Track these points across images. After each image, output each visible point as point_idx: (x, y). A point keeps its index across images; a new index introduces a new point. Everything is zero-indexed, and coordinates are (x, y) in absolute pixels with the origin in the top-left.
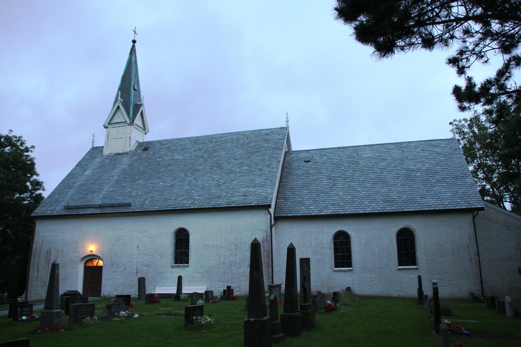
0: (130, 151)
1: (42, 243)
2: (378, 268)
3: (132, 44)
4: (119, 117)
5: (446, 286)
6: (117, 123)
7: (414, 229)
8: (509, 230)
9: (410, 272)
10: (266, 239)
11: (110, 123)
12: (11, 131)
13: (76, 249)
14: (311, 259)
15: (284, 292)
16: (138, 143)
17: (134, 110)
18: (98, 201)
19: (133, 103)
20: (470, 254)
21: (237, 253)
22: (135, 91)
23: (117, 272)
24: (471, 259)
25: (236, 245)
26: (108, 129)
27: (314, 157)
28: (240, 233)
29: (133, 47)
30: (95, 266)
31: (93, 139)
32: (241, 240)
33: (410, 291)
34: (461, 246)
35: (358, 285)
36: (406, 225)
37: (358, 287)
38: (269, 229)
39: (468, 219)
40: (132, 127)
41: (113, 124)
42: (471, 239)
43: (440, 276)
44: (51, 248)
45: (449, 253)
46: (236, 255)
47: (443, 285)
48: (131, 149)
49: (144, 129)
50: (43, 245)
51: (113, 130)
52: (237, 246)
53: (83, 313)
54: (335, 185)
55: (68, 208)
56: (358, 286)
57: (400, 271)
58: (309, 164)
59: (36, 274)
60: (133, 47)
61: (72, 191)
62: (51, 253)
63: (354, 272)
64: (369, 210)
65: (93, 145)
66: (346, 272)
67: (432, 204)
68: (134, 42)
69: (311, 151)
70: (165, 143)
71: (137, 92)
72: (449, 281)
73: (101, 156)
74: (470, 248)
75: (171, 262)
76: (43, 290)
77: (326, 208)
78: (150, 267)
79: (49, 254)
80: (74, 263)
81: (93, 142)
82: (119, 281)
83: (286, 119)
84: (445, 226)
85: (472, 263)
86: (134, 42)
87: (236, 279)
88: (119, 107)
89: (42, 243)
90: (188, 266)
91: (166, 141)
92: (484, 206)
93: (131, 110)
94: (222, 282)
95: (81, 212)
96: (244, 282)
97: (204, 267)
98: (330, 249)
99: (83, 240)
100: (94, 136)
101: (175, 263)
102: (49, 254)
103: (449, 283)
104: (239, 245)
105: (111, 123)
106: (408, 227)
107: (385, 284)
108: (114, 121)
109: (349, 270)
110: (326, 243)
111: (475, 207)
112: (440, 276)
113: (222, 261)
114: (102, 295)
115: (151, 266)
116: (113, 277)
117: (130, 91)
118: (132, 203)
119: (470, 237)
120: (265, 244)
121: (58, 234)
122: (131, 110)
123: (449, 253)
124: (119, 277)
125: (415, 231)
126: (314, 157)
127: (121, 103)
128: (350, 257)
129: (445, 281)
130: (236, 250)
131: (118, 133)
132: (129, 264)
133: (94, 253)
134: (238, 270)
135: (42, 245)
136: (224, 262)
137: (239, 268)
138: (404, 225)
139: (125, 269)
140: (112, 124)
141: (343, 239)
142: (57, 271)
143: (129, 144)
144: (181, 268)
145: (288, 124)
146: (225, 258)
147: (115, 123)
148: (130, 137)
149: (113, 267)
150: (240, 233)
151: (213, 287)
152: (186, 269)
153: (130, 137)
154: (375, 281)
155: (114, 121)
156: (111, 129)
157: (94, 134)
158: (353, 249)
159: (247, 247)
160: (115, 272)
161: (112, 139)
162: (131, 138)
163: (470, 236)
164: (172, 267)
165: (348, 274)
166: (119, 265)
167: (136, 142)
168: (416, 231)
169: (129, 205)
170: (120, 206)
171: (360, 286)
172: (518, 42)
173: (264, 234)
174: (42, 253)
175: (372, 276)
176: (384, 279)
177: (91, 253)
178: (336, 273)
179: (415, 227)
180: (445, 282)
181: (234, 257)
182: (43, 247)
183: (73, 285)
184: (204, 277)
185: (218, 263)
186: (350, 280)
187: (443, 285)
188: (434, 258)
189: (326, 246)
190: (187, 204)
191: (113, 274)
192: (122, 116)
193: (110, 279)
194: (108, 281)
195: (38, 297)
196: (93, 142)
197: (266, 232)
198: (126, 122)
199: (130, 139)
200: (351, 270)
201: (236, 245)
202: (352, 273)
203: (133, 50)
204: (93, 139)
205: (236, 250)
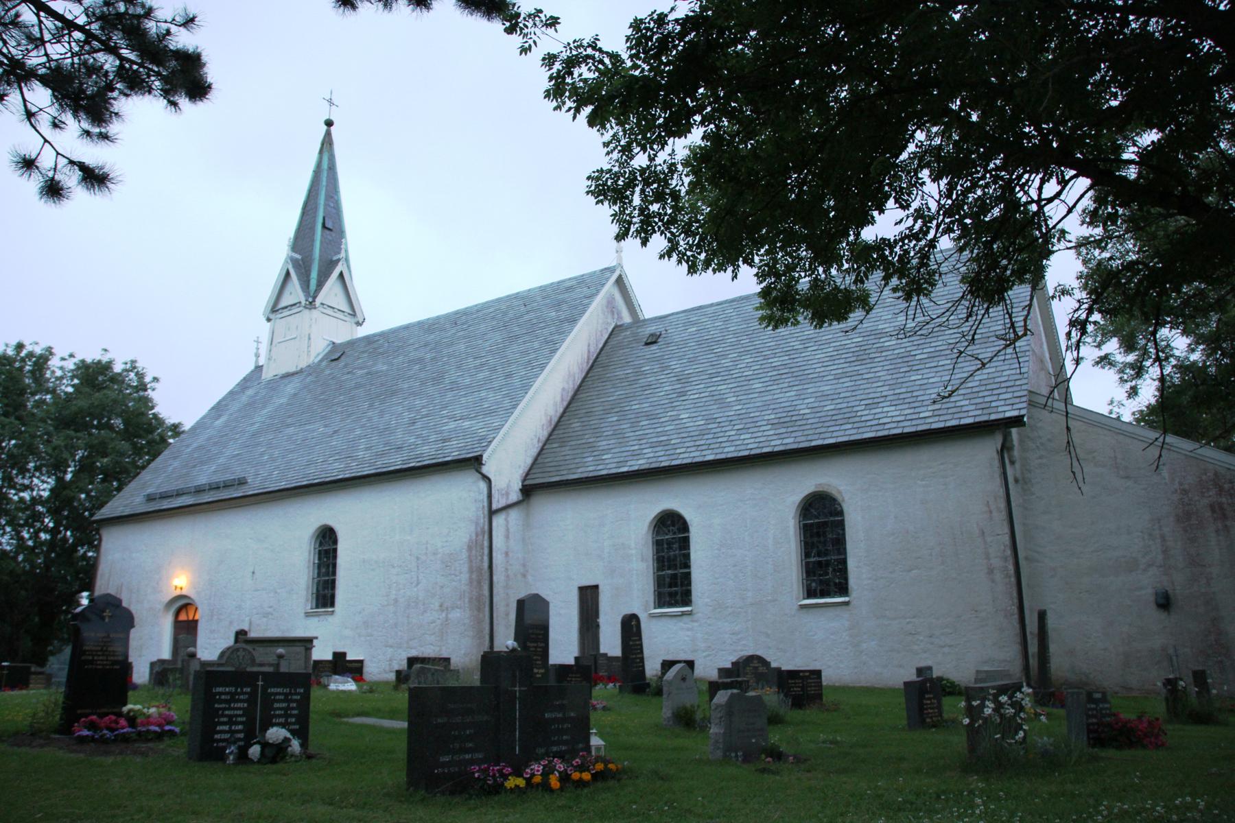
0: (309, 366)
2: (752, 604)
3: (325, 127)
4: (291, 293)
5: (925, 652)
6: (286, 307)
7: (840, 492)
8: (1127, 477)
9: (831, 612)
10: (476, 541)
11: (275, 309)
12: (106, 350)
14: (601, 588)
15: (406, 666)
16: (332, 345)
17: (319, 275)
18: (202, 479)
19: (320, 260)
20: (988, 557)
21: (420, 578)
22: (328, 232)
24: (991, 571)
25: (418, 558)
26: (272, 321)
27: (669, 331)
28: (428, 528)
29: (328, 135)
31: (258, 349)
32: (428, 546)
33: (830, 667)
34: (962, 534)
35: (704, 652)
36: (820, 484)
37: (705, 657)
38: (487, 520)
39: (985, 451)
40: (315, 313)
42: (991, 512)
43: (908, 623)
45: (931, 555)
46: (418, 584)
47: (916, 647)
48: (310, 361)
49: (354, 314)
51: (280, 323)
52: (419, 562)
53: (457, 745)
54: (683, 394)
55: (150, 498)
56: (704, 654)
57: (805, 610)
58: (652, 349)
60: (328, 135)
61: (176, 464)
63: (695, 617)
64: (730, 451)
65: (257, 361)
66: (679, 618)
67: (894, 419)
68: (329, 123)
69: (669, 318)
70: (377, 338)
71: (334, 235)
72: (931, 637)
73: (259, 384)
74: (989, 539)
75: (306, 605)
77: (636, 455)
78: (270, 616)
83: (255, 351)
84: (922, 480)
85: (993, 581)
86: (329, 123)
87: (416, 641)
90: (333, 611)
91: (374, 335)
92: (1023, 412)
93: (314, 275)
94: (391, 647)
95: (166, 505)
96: (432, 647)
97: (360, 613)
98: (642, 561)
100: (258, 342)
101: (317, 607)
103: (932, 644)
104: (423, 558)
106: (825, 489)
107: (769, 648)
108: (283, 303)
109: (683, 614)
110: (633, 545)
111: (1001, 416)
112: (908, 623)
113: (394, 597)
115: (272, 614)
117: (314, 234)
119: (989, 507)
120: (474, 552)
122: (314, 275)
123: (931, 555)
125: (843, 500)
126: (669, 331)
128: (687, 578)
129: (922, 638)
130: (418, 569)
133: (184, 592)
134: (421, 617)
136: (396, 601)
137: (422, 614)
138: (816, 486)
140: (278, 310)
141: (675, 533)
142: (945, 682)
143: (306, 350)
144: (322, 618)
145: (620, 258)
146: (399, 590)
147: (283, 308)
148: (309, 335)
150: (428, 528)
151: (374, 660)
152: (330, 618)
153: (309, 335)
154: (744, 642)
155: (283, 303)
156: (278, 321)
157: (258, 337)
158: (851, 564)
159: (439, 562)
162: (312, 337)
163: (988, 504)
164: (308, 615)
165: (681, 624)
167: (329, 345)
168: (846, 499)
169: (242, 482)
170: (227, 485)
171: (709, 655)
172: (143, 6)
173: (473, 528)
175: (736, 628)
176: (768, 635)
177: (178, 592)
178: (654, 621)
179: (841, 488)
180: (922, 641)
181: (415, 587)
184: (360, 636)
185: (386, 603)
186: (686, 638)
187: (916, 647)
188: (891, 572)
189: (634, 552)
190: (338, 470)
192: (295, 293)
197: (477, 524)
199: (309, 339)
200: (690, 613)
201: (418, 558)
202: (693, 621)
204: (258, 349)
205: (418, 569)
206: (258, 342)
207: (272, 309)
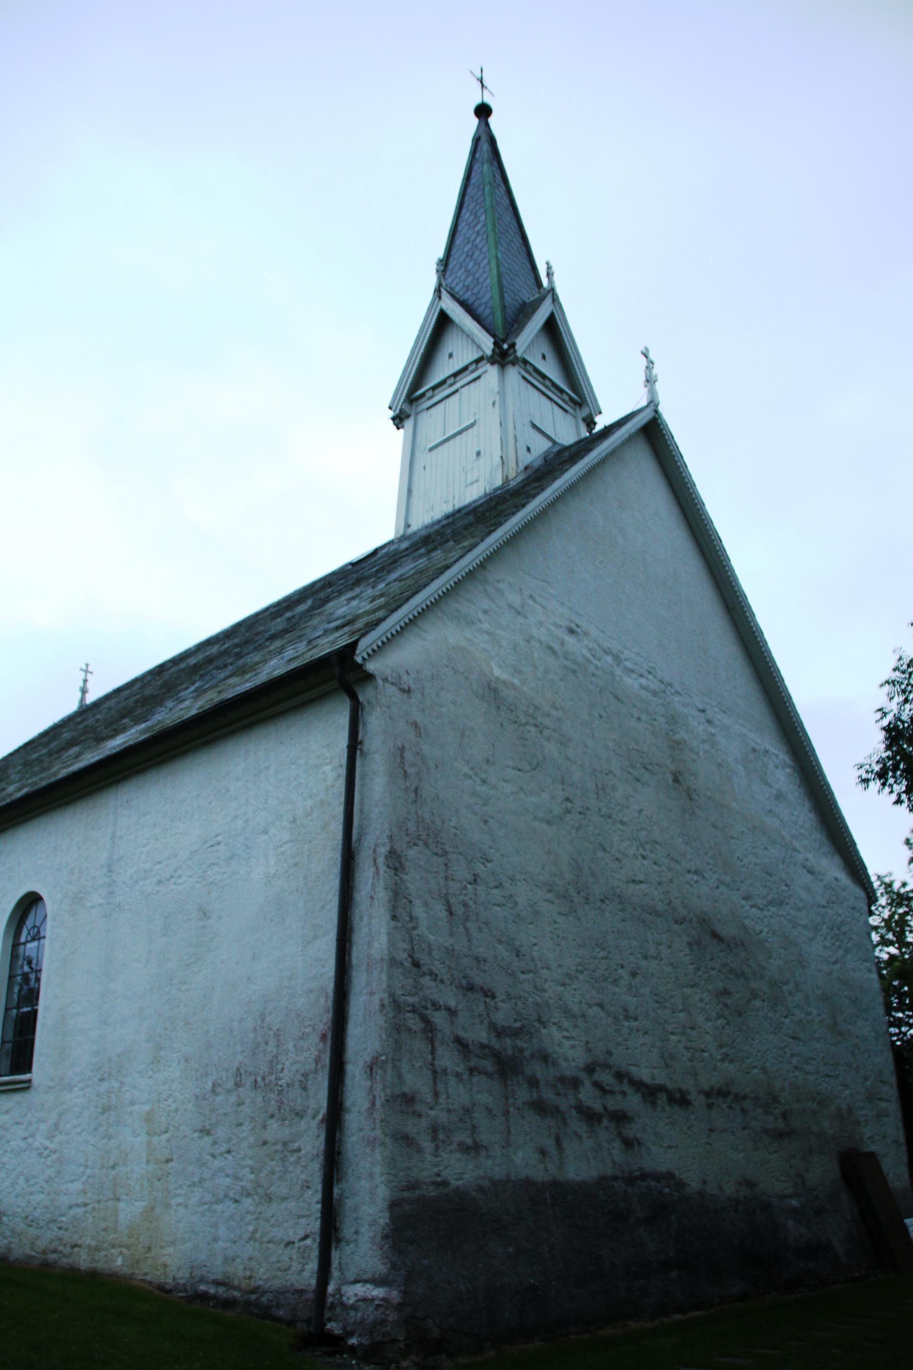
31: (85, 681)
65: (83, 699)
68: (483, 111)
81: (84, 691)
83: (81, 684)
86: (483, 111)
100: (86, 671)
157: (87, 665)
196: (84, 691)
204: (85, 681)
206: (86, 671)
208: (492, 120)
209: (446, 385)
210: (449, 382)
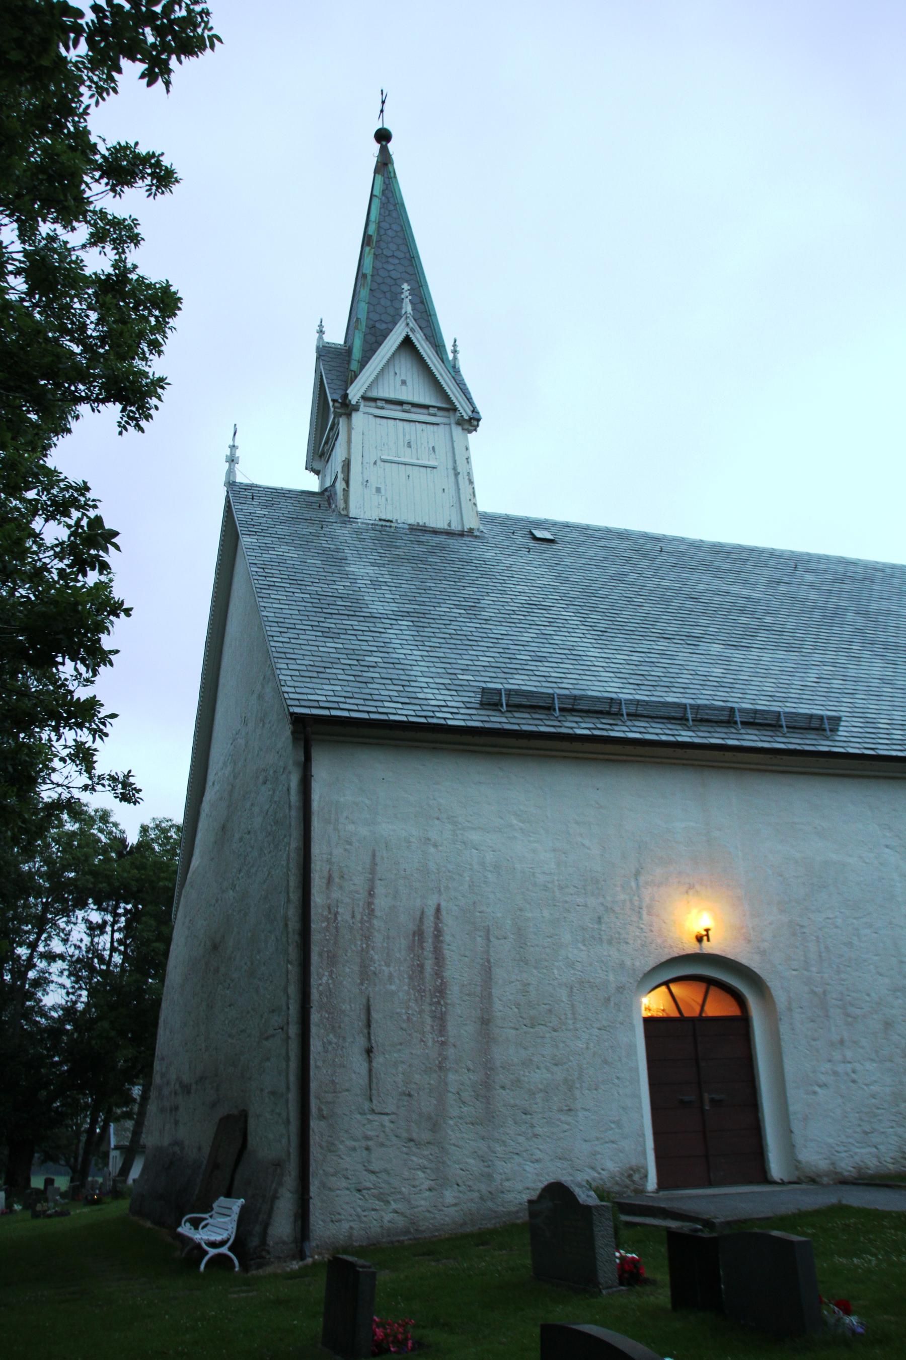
1: (372, 881)
3: (377, 147)
6: (400, 403)
13: (599, 920)
23: (855, 1042)
29: (384, 152)
30: (692, 1020)
41: (380, 404)
44: (438, 910)
50: (380, 890)
59: (358, 1062)
62: (447, 938)
65: (231, 472)
68: (383, 136)
76: (423, 1168)
79: (429, 945)
80: (608, 1000)
81: (232, 460)
82: (874, 1088)
83: (228, 452)
86: (383, 136)
88: (407, 343)
89: (372, 881)
99: (637, 874)
102: (429, 945)
105: (374, 394)
114: (776, 1168)
116: (840, 1068)
118: (843, 719)
121: (475, 836)
124: (868, 1065)
127: (417, 329)
131: (409, 445)
132: (900, 1001)
135: (371, 893)
139: (888, 1025)
140: (375, 400)
149: (827, 1016)
160: (842, 1042)
161: (384, 461)
166: (852, 1005)
174: (378, 939)
177: (692, 947)
182: (381, 903)
183: (618, 1124)
191: (837, 1056)
193: (823, 1078)
194: (815, 1093)
195: (388, 1217)
196: (232, 460)
198: (455, 409)
203: (384, 164)
207: (370, 387)
208: (391, 146)
209: (399, 408)
210: (406, 407)
